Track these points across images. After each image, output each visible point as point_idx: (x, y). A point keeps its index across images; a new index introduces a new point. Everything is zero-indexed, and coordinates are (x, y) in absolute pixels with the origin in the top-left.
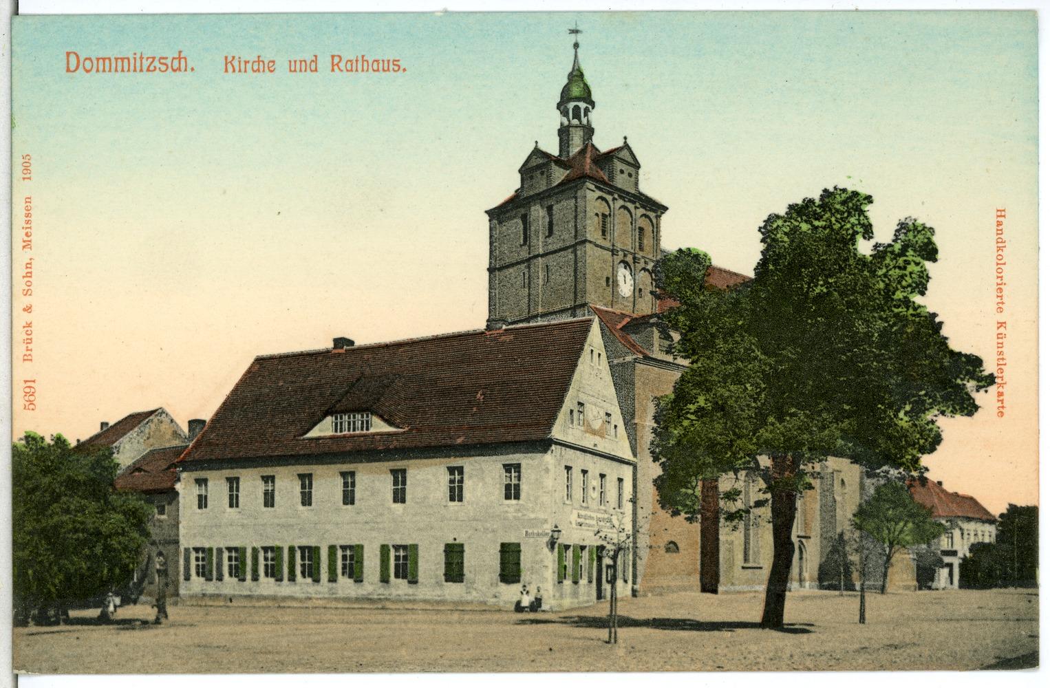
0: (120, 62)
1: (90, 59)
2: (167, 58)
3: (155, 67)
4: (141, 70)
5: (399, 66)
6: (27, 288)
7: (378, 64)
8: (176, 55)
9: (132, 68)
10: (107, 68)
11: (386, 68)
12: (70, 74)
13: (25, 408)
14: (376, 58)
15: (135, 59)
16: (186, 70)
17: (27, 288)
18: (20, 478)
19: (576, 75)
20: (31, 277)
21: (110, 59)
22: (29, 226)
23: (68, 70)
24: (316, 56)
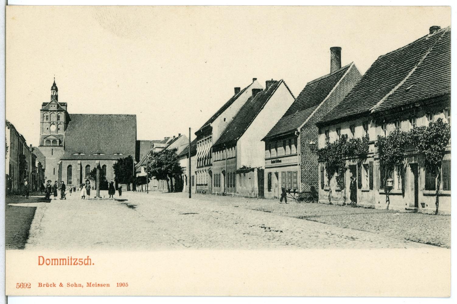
0: (62, 260)
1: (49, 259)
2: (82, 259)
3: (77, 263)
4: (71, 264)
6: (70, 284)
9: (67, 263)
10: (64, 263)
12: (40, 266)
13: (17, 283)
15: (68, 259)
16: (90, 264)
17: (70, 285)
19: (54, 84)
20: (75, 286)
21: (57, 259)
22: (97, 285)
23: (39, 264)
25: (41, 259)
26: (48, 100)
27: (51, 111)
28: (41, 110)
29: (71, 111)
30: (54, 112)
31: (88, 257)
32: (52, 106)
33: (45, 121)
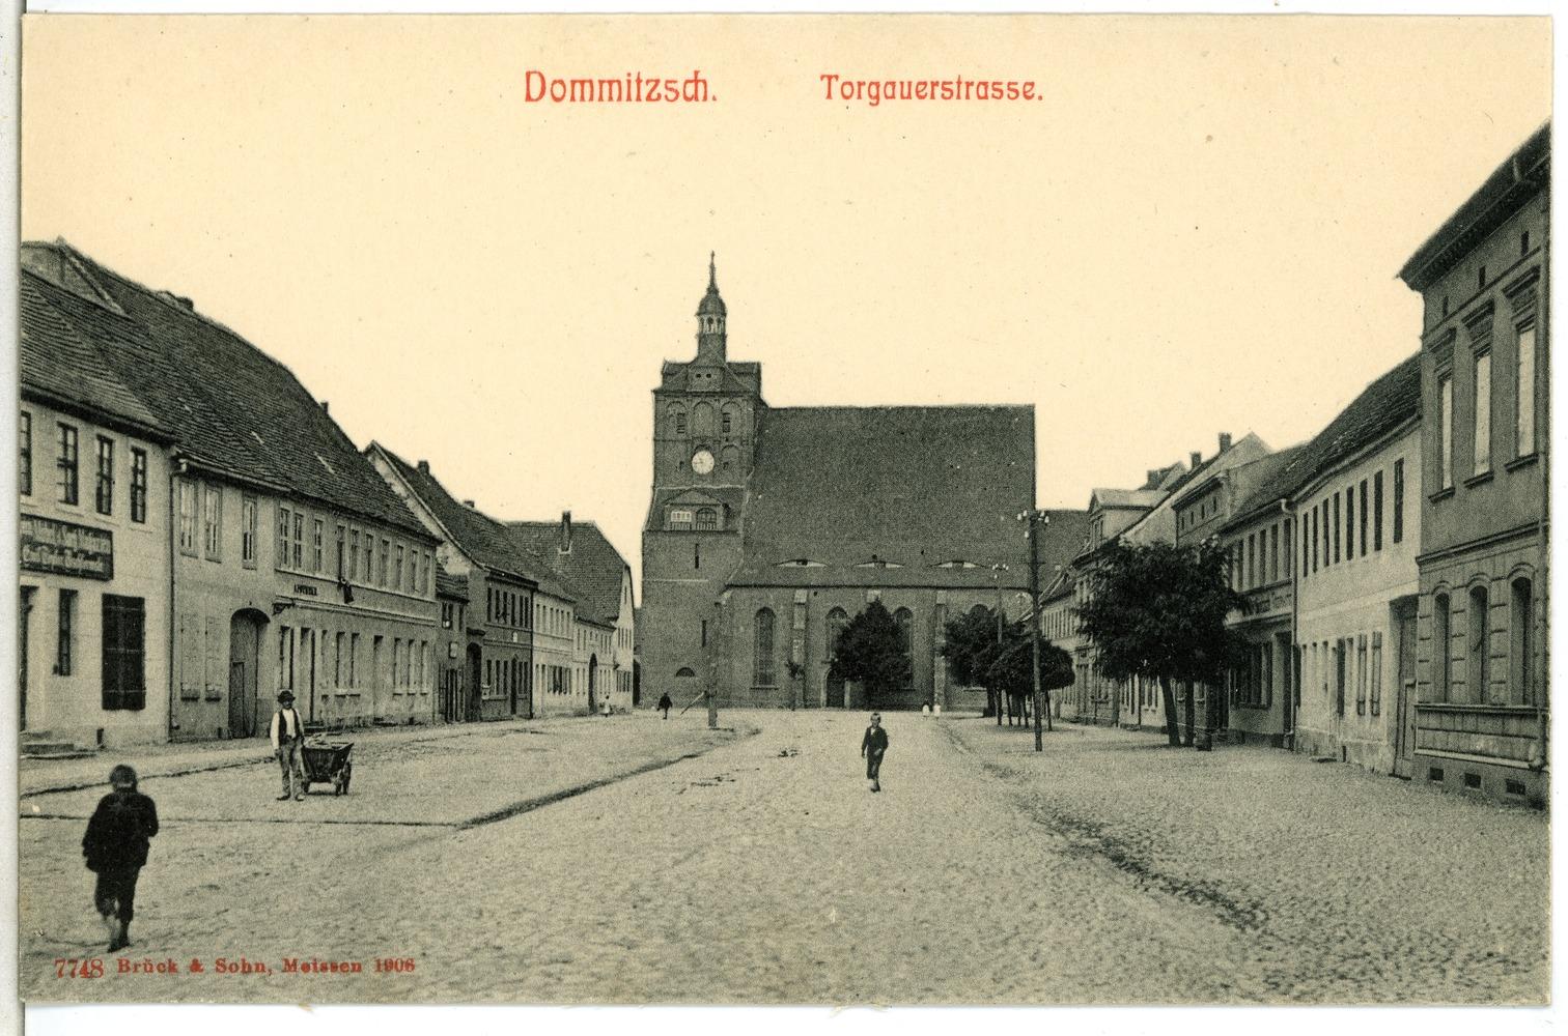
0: (606, 87)
1: (561, 82)
3: (659, 96)
4: (639, 99)
5: (1016, 91)
7: (986, 89)
8: (692, 77)
10: (587, 96)
11: (906, 94)
14: (983, 79)
15: (629, 82)
16: (705, 98)
18: (1539, 954)
19: (713, 290)
23: (528, 98)
24: (822, 77)
25: (535, 79)
26: (687, 352)
27: (696, 394)
28: (656, 392)
29: (777, 393)
30: (707, 399)
31: (696, 73)
32: (699, 376)
33: (672, 433)
